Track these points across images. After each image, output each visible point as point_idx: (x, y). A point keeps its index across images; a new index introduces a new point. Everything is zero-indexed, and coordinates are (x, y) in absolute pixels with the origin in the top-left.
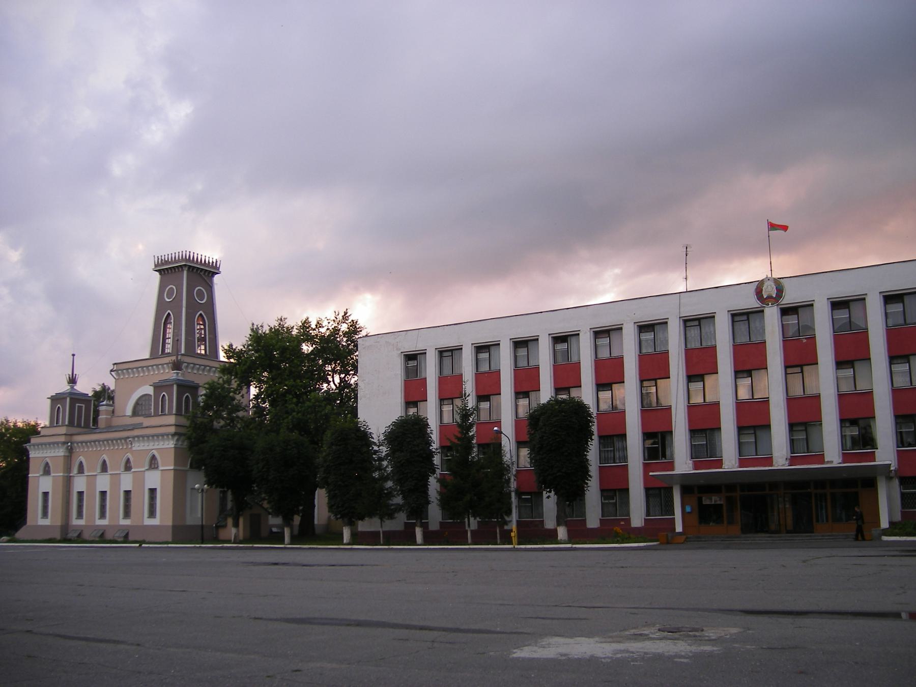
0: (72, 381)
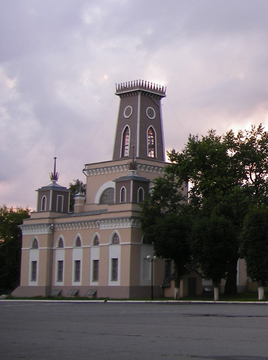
0: (55, 177)
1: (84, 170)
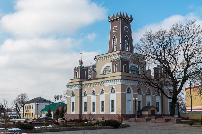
0: (81, 62)
1: (95, 59)
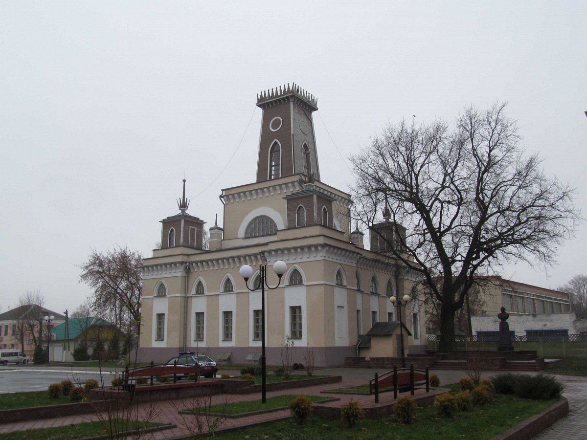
0: (183, 206)
